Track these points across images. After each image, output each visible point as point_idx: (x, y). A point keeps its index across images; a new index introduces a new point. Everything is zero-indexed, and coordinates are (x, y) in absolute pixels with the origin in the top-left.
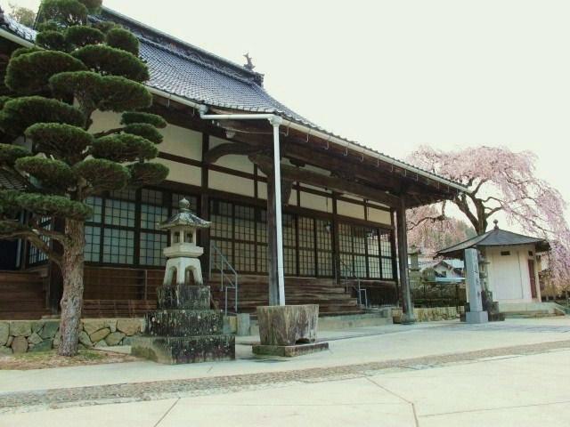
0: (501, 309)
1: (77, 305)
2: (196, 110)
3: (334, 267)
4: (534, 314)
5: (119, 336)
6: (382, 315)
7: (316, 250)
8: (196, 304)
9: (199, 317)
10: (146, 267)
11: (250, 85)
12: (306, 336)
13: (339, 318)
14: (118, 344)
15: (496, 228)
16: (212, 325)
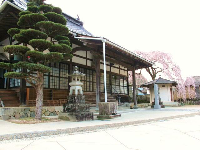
0: (164, 104)
1: (42, 102)
3: (110, 90)
4: (172, 106)
5: (49, 113)
6: (127, 106)
8: (81, 101)
10: (52, 89)
11: (79, 26)
12: (115, 112)
14: (48, 115)
15: (160, 78)
16: (87, 109)
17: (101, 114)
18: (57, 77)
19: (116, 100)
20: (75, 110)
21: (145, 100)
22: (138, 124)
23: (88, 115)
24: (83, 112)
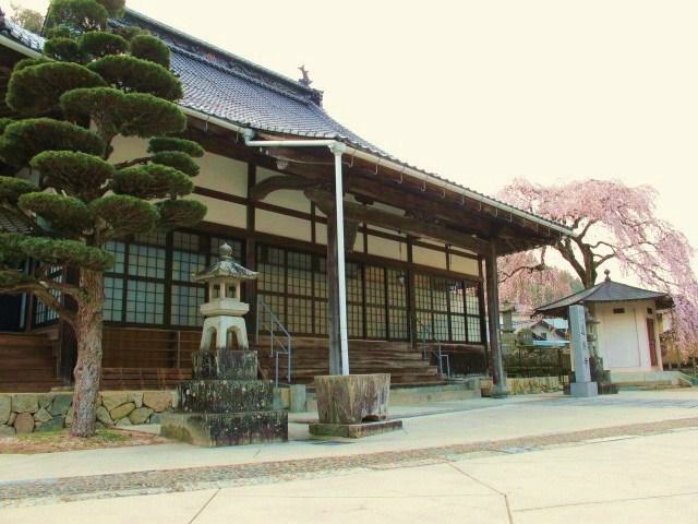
0: (614, 380)
2: (240, 135)
4: (652, 387)
6: (468, 386)
9: (244, 389)
11: (306, 105)
12: (375, 412)
13: (415, 390)
14: (145, 422)
16: (260, 399)
17: (325, 419)
18: (156, 281)
19: (432, 364)
20: (211, 402)
22: (393, 465)
23: (265, 423)
24: (245, 410)
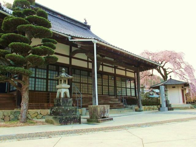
0: (172, 106)
1: (27, 105)
2: (68, 38)
3: (115, 92)
4: (183, 108)
6: (131, 108)
7: (109, 86)
8: (67, 104)
10: (50, 92)
11: (86, 29)
12: (105, 116)
13: (116, 109)
14: (41, 118)
16: (73, 112)
17: (91, 118)
18: (44, 79)
20: (59, 113)
21: (156, 102)
24: (69, 115)
